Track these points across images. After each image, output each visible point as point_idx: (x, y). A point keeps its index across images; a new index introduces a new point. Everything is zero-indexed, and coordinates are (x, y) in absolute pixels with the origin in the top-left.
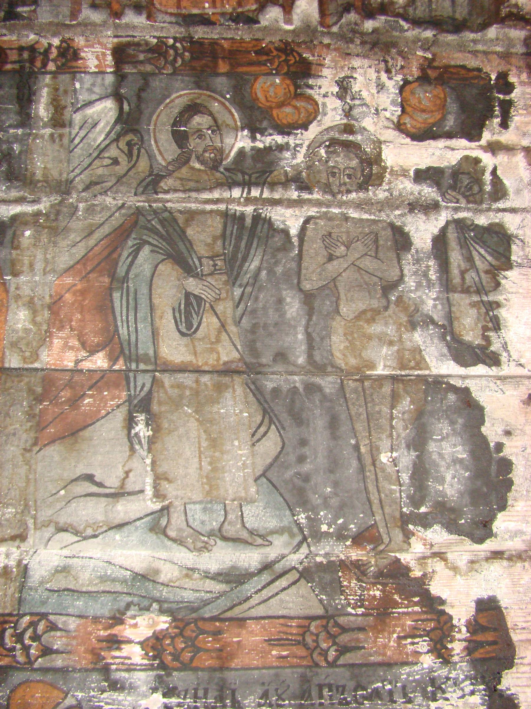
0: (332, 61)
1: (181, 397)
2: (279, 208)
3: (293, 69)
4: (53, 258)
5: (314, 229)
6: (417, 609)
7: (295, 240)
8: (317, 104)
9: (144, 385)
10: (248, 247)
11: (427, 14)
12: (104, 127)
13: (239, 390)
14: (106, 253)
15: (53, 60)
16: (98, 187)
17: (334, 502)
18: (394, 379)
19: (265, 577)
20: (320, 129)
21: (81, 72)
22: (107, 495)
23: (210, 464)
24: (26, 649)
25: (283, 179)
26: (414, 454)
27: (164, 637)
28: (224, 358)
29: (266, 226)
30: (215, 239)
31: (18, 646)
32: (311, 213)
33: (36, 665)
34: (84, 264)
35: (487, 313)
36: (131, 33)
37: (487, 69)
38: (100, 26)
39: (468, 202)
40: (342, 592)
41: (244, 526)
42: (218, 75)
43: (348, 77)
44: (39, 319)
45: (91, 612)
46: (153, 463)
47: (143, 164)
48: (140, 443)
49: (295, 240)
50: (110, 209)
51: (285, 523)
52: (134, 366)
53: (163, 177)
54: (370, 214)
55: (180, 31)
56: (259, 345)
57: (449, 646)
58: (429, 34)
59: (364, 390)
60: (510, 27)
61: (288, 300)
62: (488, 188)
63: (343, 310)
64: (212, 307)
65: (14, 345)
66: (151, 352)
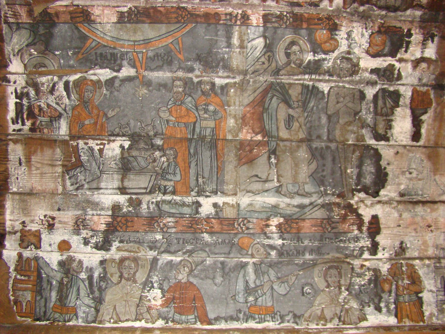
0: (346, 24)
1: (286, 149)
2: (321, 83)
3: (331, 27)
4: (242, 100)
5: (333, 91)
6: (355, 217)
7: (326, 96)
8: (338, 42)
9: (273, 146)
10: (310, 98)
11: (385, 4)
12: (259, 49)
13: (305, 148)
14: (261, 99)
15: (239, 20)
16: (257, 73)
17: (332, 184)
18: (354, 145)
19: (311, 207)
20: (338, 52)
21: (250, 26)
22: (262, 181)
23: (295, 172)
24: (242, 228)
25: (324, 72)
26: (358, 170)
27: (282, 224)
28: (300, 137)
29: (316, 90)
30: (299, 94)
31: (239, 227)
32: (332, 85)
33: (245, 232)
34: (253, 103)
35: (388, 123)
36: (270, 9)
37: (404, 27)
38: (258, 6)
39: (388, 81)
40: (333, 212)
41: (304, 190)
42: (303, 29)
43: (351, 31)
44: (238, 122)
45: (260, 217)
46: (277, 171)
47: (274, 65)
48: (273, 165)
49: (326, 96)
50: (262, 82)
51: (317, 190)
52: (270, 139)
53: (281, 70)
54: (353, 86)
55: (288, 9)
56: (312, 133)
57: (363, 228)
58: (384, 13)
59: (344, 148)
60: (416, 10)
61: (323, 117)
62: (396, 76)
63: (341, 121)
64: (297, 119)
65: (229, 131)
66: (276, 135)
